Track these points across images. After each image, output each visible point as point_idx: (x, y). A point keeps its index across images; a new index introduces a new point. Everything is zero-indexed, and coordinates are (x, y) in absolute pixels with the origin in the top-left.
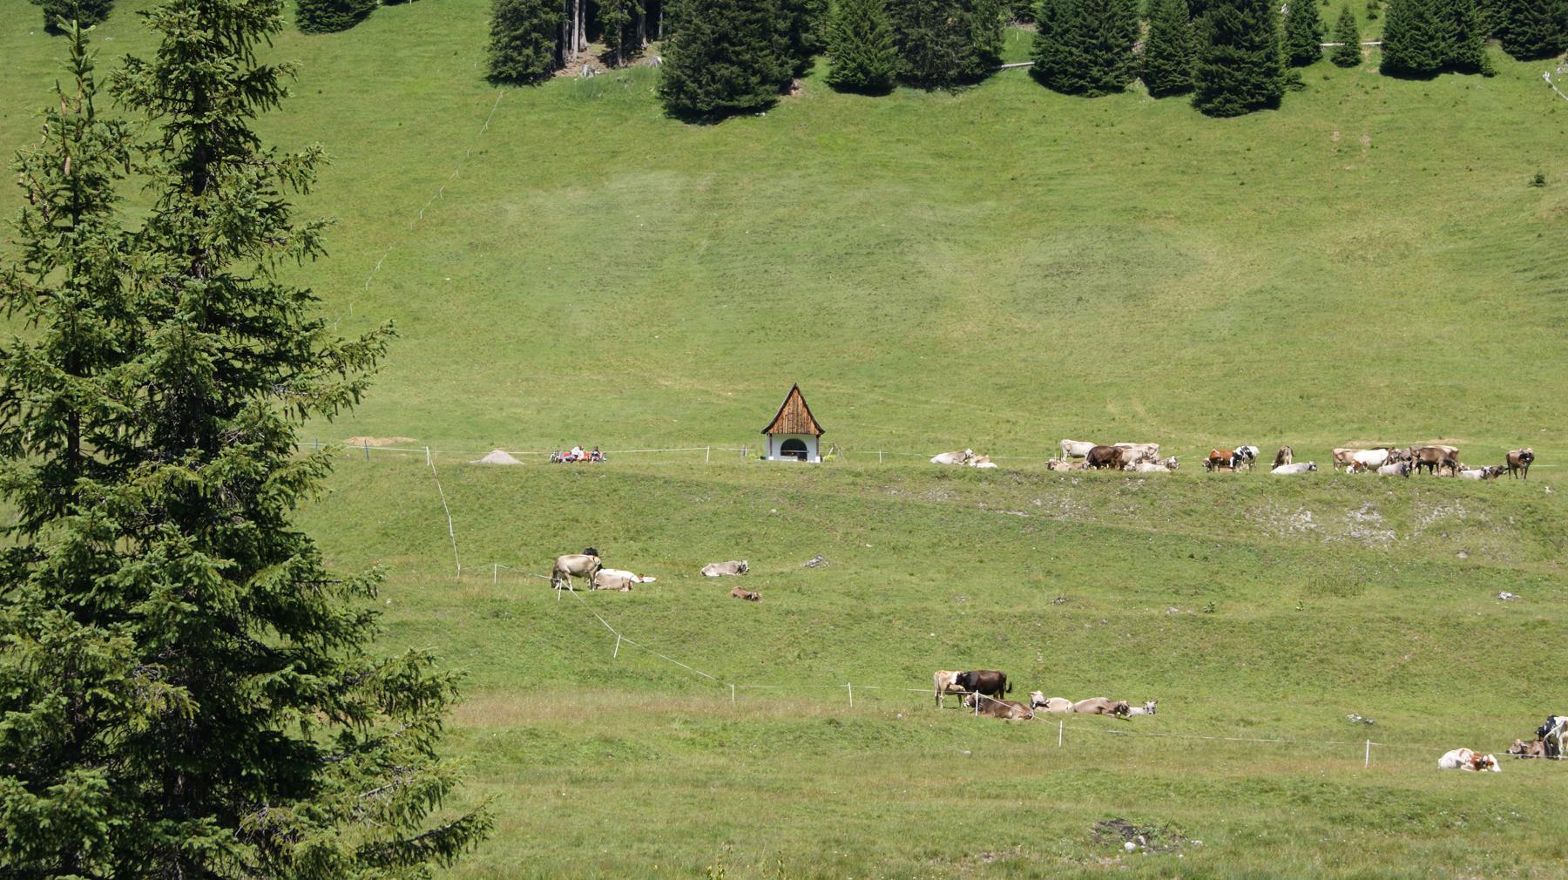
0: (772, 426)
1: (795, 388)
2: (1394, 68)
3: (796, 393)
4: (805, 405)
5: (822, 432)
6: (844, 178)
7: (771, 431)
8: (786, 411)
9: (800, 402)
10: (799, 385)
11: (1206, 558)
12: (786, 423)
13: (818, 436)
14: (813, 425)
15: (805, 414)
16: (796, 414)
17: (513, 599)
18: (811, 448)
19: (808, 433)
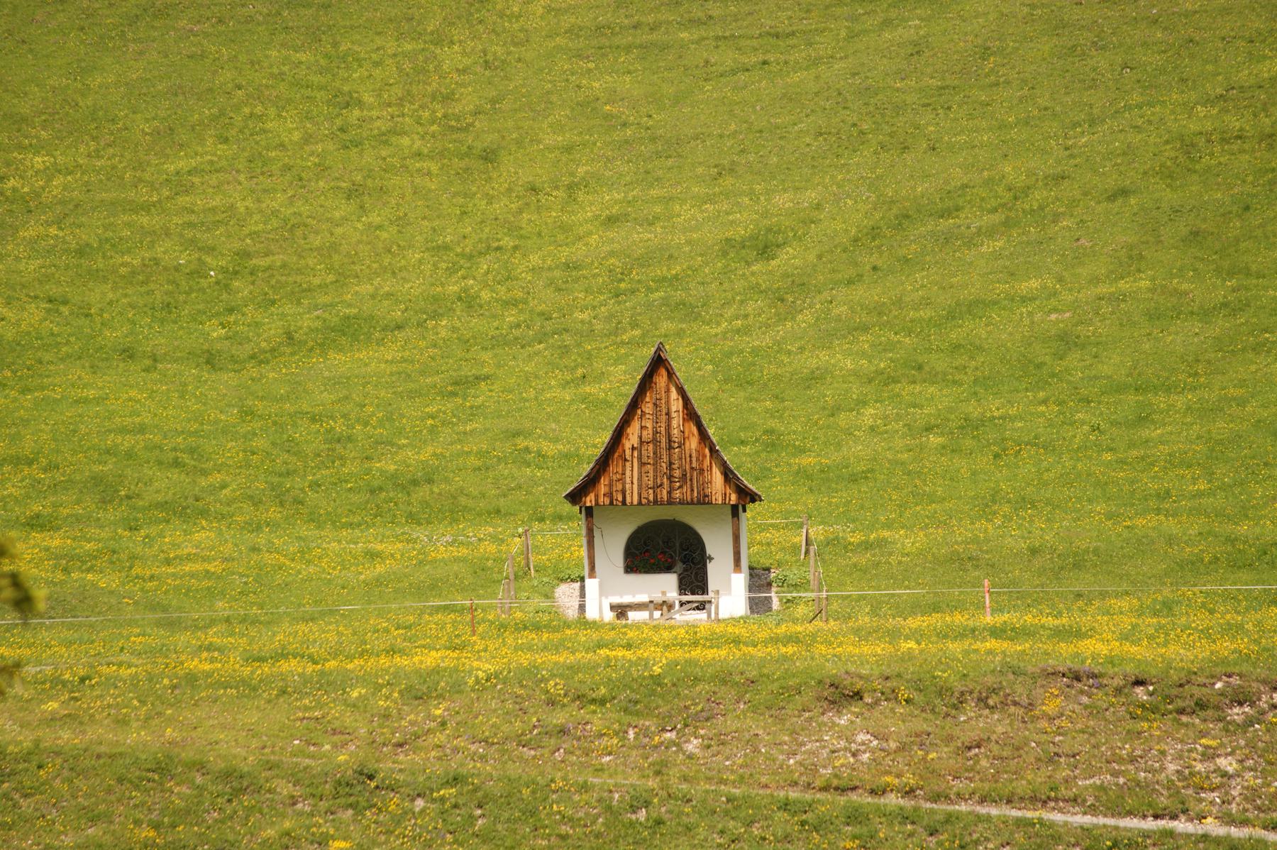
0: (590, 483)
1: (658, 362)
2: (704, 590)
3: (661, 379)
4: (691, 414)
5: (748, 496)
6: (293, 662)
7: (589, 500)
8: (633, 436)
9: (676, 405)
10: (669, 356)
11: (82, 29)
12: (632, 472)
13: (735, 511)
14: (717, 477)
15: (693, 443)
16: (664, 443)
17: (30, 744)
18: (717, 545)
19: (703, 501)
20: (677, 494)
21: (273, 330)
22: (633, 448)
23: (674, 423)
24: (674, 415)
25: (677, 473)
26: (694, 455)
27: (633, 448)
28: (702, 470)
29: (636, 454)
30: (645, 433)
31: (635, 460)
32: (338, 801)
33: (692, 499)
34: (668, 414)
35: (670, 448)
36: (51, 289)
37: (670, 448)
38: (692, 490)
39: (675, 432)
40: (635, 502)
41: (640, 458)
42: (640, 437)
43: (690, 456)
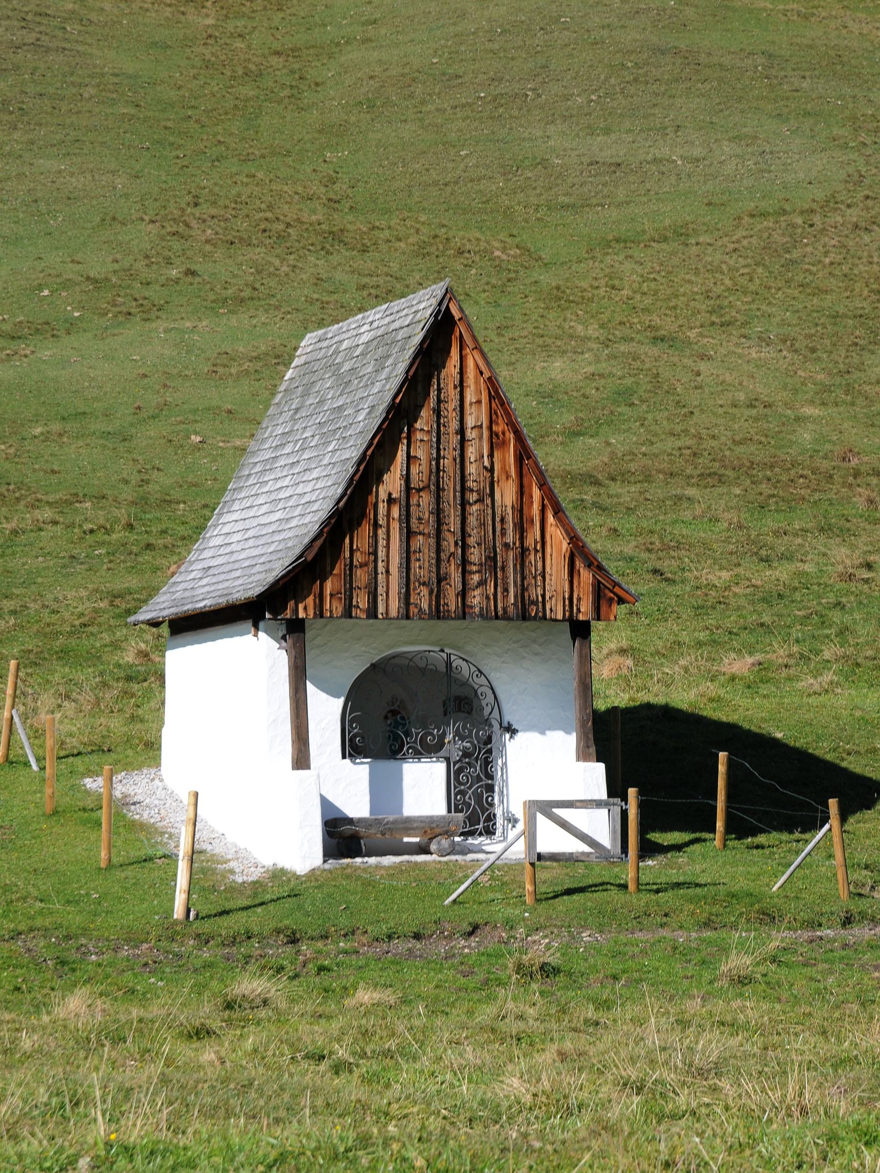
20: (476, 599)
21: (89, 749)
22: (390, 501)
23: (471, 453)
24: (470, 434)
25: (475, 555)
26: (510, 518)
27: (390, 501)
28: (524, 551)
29: (395, 512)
30: (414, 470)
31: (395, 526)
32: (769, 310)
33: (505, 609)
34: (462, 431)
35: (464, 503)
36: (743, 1009)
37: (464, 503)
38: (506, 590)
39: (472, 469)
40: (393, 613)
41: (407, 516)
42: (407, 478)
43: (503, 520)
